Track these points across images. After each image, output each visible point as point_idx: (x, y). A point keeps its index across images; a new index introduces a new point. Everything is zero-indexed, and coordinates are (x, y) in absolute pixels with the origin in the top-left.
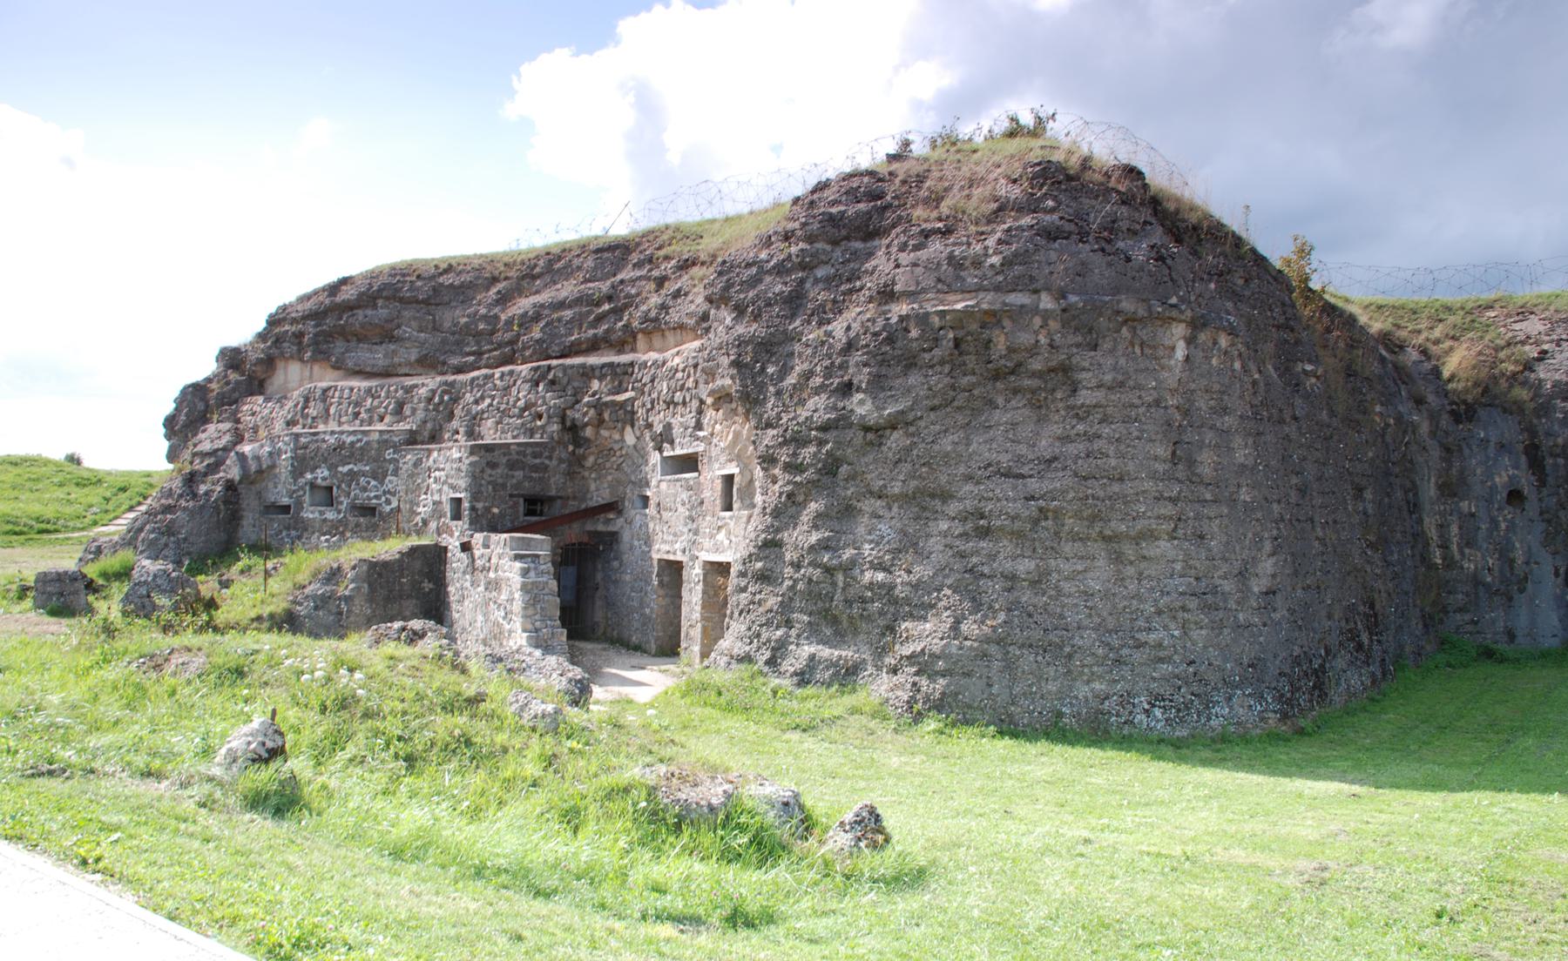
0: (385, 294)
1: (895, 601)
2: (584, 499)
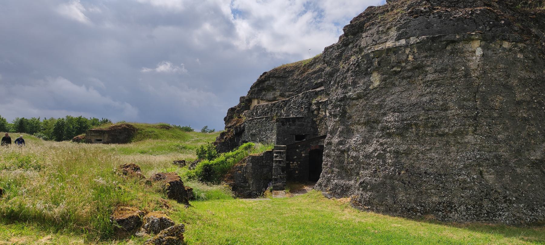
0: (271, 76)
1: (359, 163)
2: (317, 135)
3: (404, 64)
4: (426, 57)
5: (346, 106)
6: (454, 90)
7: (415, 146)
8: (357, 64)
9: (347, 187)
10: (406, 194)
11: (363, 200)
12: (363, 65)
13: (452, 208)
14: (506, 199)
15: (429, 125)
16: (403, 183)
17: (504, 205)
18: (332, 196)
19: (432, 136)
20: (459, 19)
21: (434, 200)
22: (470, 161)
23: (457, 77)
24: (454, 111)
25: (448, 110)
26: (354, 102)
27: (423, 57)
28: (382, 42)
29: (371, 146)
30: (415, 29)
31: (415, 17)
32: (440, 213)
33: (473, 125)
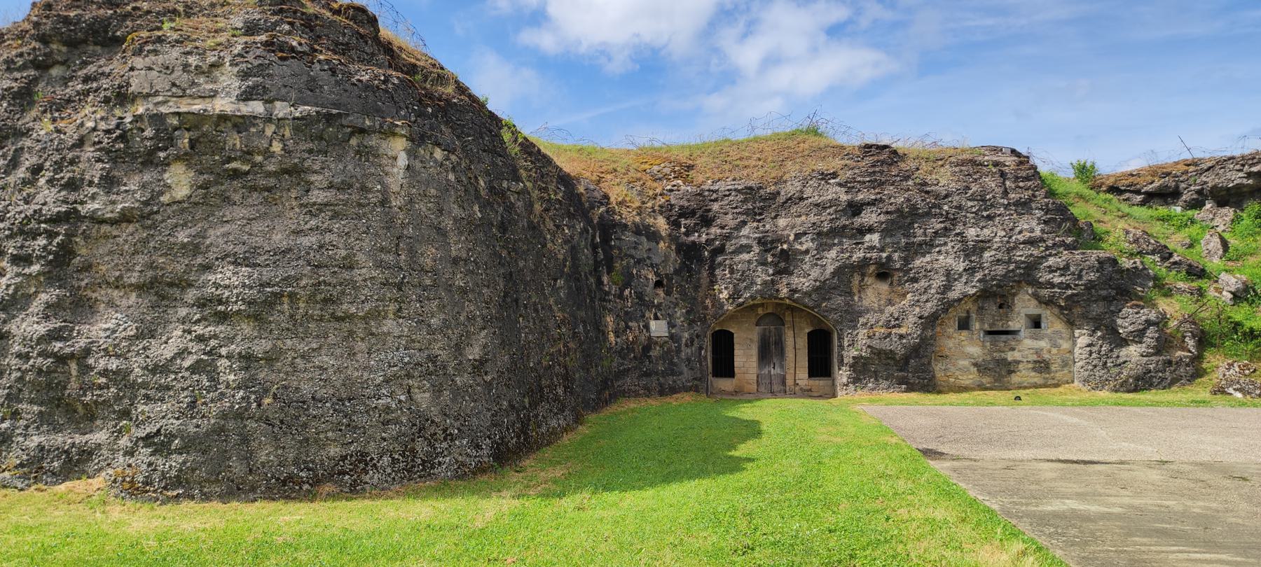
3: (259, 158)
4: (310, 151)
5: (76, 236)
6: (365, 229)
7: (289, 342)
8: (118, 131)
9: (84, 451)
10: (276, 449)
11: (156, 477)
12: (138, 139)
13: (366, 465)
14: (448, 437)
15: (319, 297)
16: (270, 424)
17: (445, 445)
18: (32, 481)
19: (321, 320)
20: (367, 87)
21: (332, 453)
22: (395, 369)
23: (369, 204)
24: (365, 270)
25: (354, 268)
26: (105, 228)
27: (304, 151)
28: (203, 95)
29: (166, 343)
30: (286, 86)
31: (281, 59)
32: (347, 477)
33: (396, 300)
